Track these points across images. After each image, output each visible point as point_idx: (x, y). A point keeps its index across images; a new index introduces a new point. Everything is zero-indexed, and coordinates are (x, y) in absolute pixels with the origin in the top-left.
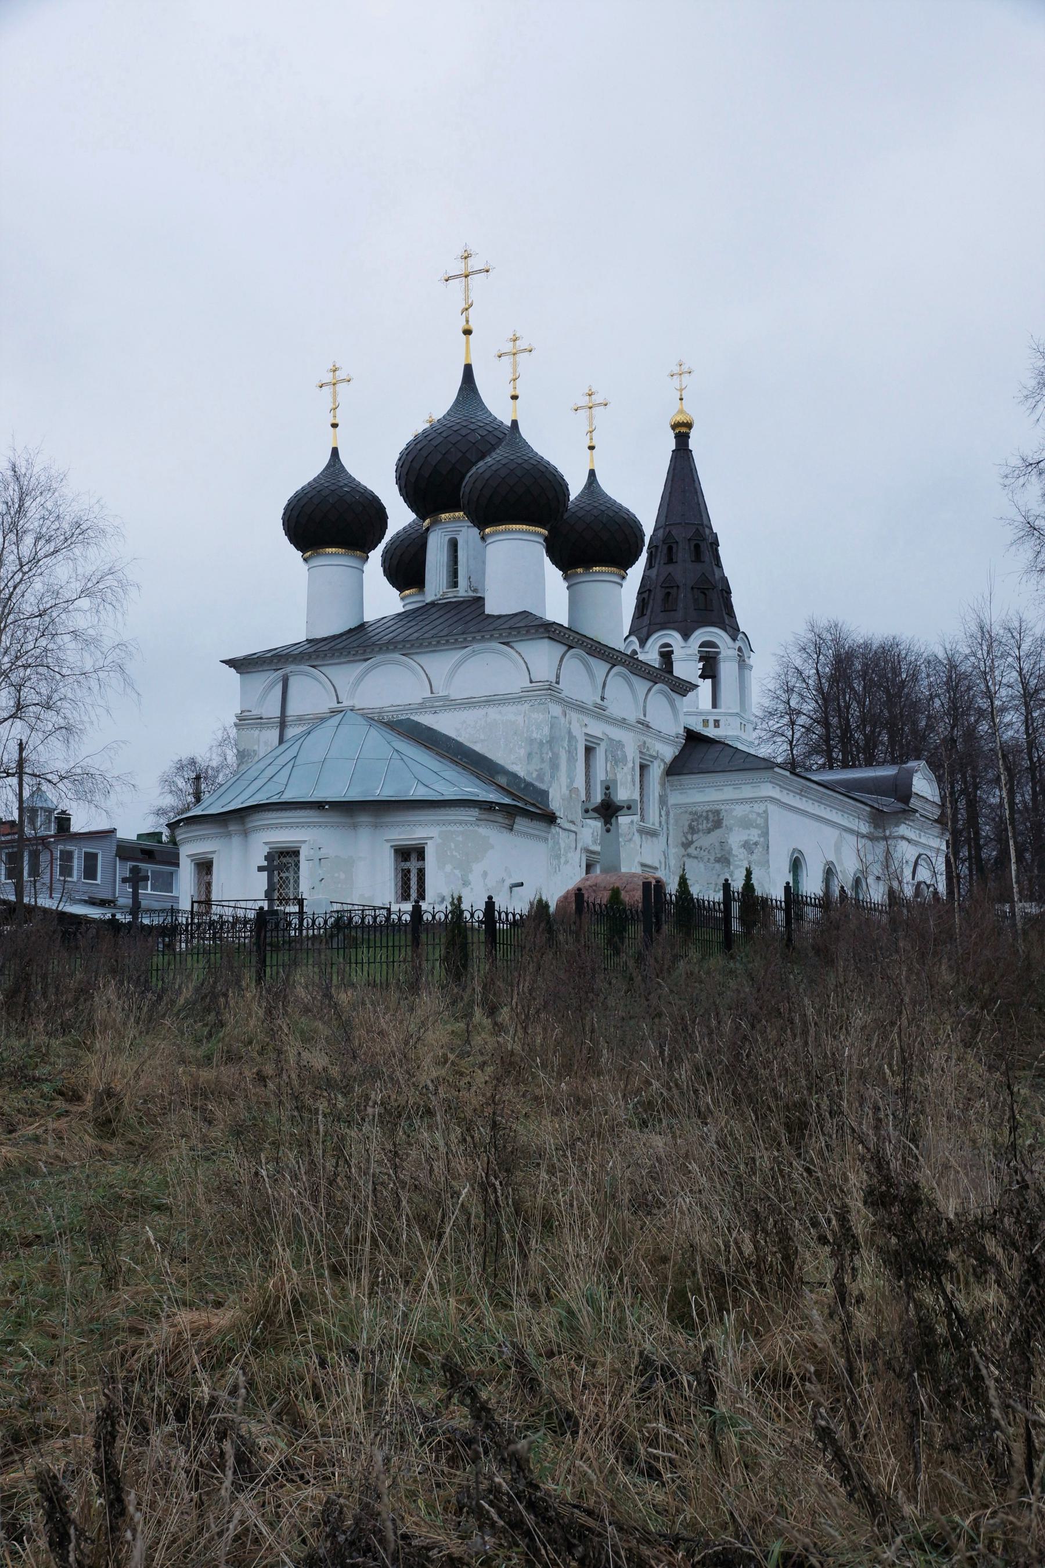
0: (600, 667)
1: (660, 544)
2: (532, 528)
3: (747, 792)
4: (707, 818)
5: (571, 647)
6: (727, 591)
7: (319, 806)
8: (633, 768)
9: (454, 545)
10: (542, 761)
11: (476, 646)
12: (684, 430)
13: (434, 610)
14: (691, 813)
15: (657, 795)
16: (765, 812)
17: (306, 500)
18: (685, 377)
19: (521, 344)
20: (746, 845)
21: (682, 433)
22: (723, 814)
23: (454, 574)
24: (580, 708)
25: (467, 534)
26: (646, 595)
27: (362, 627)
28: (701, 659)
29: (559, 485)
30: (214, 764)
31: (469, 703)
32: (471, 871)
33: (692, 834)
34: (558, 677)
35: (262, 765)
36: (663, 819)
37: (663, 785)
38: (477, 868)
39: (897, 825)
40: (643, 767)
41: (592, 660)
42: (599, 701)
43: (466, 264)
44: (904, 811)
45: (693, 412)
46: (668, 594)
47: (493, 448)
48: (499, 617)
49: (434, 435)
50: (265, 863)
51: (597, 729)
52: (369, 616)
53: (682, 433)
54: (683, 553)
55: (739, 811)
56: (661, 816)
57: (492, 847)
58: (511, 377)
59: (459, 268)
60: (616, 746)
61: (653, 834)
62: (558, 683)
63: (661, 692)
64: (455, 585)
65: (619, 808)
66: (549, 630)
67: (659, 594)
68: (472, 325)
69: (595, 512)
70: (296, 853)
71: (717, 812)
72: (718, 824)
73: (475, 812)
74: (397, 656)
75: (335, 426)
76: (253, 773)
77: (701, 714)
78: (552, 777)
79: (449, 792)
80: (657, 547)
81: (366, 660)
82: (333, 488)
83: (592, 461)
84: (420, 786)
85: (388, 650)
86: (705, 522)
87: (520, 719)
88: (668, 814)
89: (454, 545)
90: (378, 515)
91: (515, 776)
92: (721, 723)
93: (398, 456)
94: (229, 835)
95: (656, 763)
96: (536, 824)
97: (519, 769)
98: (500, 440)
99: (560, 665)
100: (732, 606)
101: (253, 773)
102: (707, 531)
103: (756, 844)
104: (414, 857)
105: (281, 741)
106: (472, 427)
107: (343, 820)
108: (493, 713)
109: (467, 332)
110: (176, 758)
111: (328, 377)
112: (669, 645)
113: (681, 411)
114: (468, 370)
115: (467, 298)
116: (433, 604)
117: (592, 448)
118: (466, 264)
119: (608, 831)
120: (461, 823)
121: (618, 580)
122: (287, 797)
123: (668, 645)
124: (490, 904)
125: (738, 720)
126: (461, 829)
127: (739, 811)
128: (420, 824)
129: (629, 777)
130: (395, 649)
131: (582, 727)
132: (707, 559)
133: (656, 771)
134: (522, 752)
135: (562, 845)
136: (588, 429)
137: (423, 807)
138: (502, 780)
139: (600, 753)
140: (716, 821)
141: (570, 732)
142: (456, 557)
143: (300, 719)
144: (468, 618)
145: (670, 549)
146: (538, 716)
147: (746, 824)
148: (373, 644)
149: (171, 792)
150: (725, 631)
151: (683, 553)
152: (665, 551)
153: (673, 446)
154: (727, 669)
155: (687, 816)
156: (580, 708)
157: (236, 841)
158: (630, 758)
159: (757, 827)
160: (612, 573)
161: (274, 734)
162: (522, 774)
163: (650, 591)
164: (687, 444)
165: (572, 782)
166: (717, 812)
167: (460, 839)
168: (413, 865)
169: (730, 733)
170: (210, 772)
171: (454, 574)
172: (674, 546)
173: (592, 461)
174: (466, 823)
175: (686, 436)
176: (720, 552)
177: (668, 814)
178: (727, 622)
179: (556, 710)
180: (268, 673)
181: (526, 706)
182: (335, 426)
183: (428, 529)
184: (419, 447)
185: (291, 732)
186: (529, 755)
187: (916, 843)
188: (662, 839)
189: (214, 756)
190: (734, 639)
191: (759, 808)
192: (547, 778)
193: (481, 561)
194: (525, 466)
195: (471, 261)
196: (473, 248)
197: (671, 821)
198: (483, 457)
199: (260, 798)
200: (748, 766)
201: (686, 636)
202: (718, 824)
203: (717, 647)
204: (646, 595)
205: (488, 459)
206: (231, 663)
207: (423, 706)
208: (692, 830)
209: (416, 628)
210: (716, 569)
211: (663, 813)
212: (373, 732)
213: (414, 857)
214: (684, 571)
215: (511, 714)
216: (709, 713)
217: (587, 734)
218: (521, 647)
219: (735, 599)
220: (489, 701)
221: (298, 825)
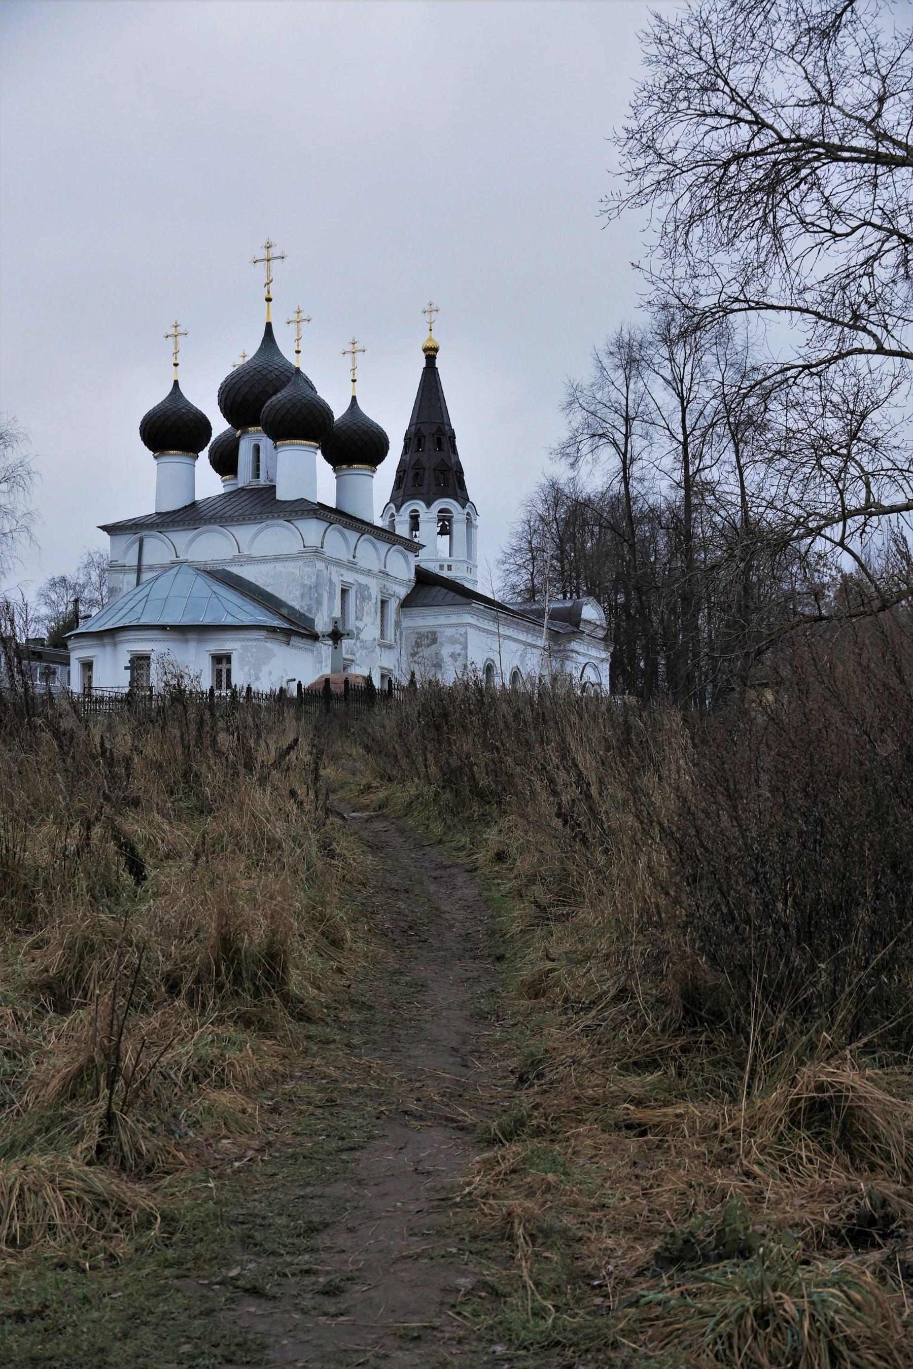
0: (353, 536)
1: (412, 437)
2: (308, 443)
3: (454, 619)
4: (427, 637)
5: (332, 524)
6: (461, 472)
7: (163, 628)
8: (376, 603)
9: (257, 449)
10: (311, 599)
11: (269, 522)
12: (432, 353)
13: (244, 493)
14: (417, 633)
15: (393, 621)
16: (466, 633)
17: (155, 418)
18: (434, 314)
19: (303, 316)
20: (453, 656)
21: (431, 354)
22: (438, 634)
23: (257, 468)
24: (338, 563)
25: (266, 443)
26: (401, 474)
27: (194, 504)
28: (440, 520)
29: (326, 412)
30: (81, 581)
31: (263, 560)
32: (261, 671)
33: (418, 647)
34: (322, 543)
35: (125, 600)
36: (398, 637)
37: (398, 615)
38: (265, 669)
39: (570, 642)
40: (383, 603)
41: (346, 531)
42: (351, 559)
43: (268, 252)
44: (574, 632)
45: (439, 340)
46: (417, 474)
47: (284, 385)
48: (285, 502)
49: (244, 373)
50: (129, 665)
51: (350, 577)
52: (199, 496)
53: (431, 354)
54: (429, 443)
55: (449, 632)
56: (396, 635)
57: (275, 656)
58: (296, 337)
59: (263, 254)
60: (363, 590)
61: (390, 647)
62: (322, 547)
63: (398, 551)
64: (258, 476)
65: (343, 635)
66: (319, 511)
67: (411, 473)
68: (272, 295)
69: (355, 427)
70: (148, 658)
71: (434, 633)
72: (434, 641)
73: (264, 633)
74: (216, 527)
75: (176, 365)
76: (120, 605)
77: (438, 560)
78: (317, 610)
79: (247, 620)
80: (410, 439)
81: (195, 529)
82: (175, 410)
83: (354, 390)
84: (229, 616)
85: (210, 523)
86: (446, 421)
87: (297, 571)
88: (401, 634)
89: (257, 449)
90: (204, 426)
91: (292, 608)
92: (453, 568)
93: (219, 386)
94: (104, 645)
95: (393, 599)
96: (305, 641)
97: (296, 605)
98: (289, 379)
99: (324, 536)
100: (464, 482)
101: (120, 605)
102: (447, 428)
103: (459, 655)
104: (224, 661)
105: (138, 584)
106: (270, 368)
107: (176, 637)
108: (279, 566)
109: (269, 300)
110: (50, 577)
111: (172, 331)
112: (417, 511)
113: (430, 339)
114: (269, 326)
115: (269, 276)
116: (242, 489)
117: (354, 381)
118: (268, 252)
119: (336, 648)
120: (255, 640)
121: (370, 473)
122: (143, 621)
123: (416, 511)
124: (249, 689)
125: (466, 566)
126: (254, 643)
127: (449, 632)
128: (228, 640)
129: (373, 609)
130: (215, 523)
131: (339, 576)
132: (446, 449)
133: (393, 605)
134: (298, 593)
135: (324, 654)
136: (352, 367)
137: (224, 630)
138: (285, 611)
139: (352, 594)
140: (433, 639)
141: (330, 580)
142: (258, 457)
143: (151, 568)
144: (266, 501)
145: (419, 441)
146: (308, 570)
147: (453, 641)
148: (201, 518)
149: (46, 603)
150: (458, 501)
151: (429, 443)
152: (416, 442)
153: (424, 364)
154: (459, 528)
155: (414, 635)
156: (338, 563)
157: (108, 649)
158: (374, 596)
159: (460, 643)
160: (366, 469)
161: (133, 577)
162: (297, 608)
163: (404, 471)
164: (434, 364)
165: (331, 613)
166: (434, 633)
167: (254, 650)
168: (224, 667)
169: (458, 575)
170: (77, 588)
171: (257, 468)
172: (423, 439)
173: (354, 390)
174: (258, 640)
175: (434, 357)
176: (457, 443)
177: (401, 634)
178: (459, 494)
179: (320, 565)
180: (127, 537)
181: (301, 563)
182: (176, 365)
183: (240, 437)
184: (234, 381)
185: (146, 576)
186: (303, 595)
187: (584, 655)
188: (397, 651)
189: (81, 576)
190: (463, 507)
191: (462, 630)
192: (314, 611)
193: (274, 460)
194: (304, 401)
195: (272, 250)
196: (273, 241)
197: (404, 639)
198: (277, 391)
199: (125, 622)
200: (455, 602)
201: (429, 504)
202: (434, 641)
203: (451, 512)
204: (401, 474)
205: (279, 395)
206: (104, 528)
207: (233, 561)
208: (418, 645)
209: (228, 503)
210: (452, 455)
211: (398, 633)
212: (199, 579)
213: (224, 661)
214: (430, 457)
215: (292, 568)
216: (445, 560)
217: (342, 581)
218: (297, 523)
219: (467, 478)
220: (277, 559)
221: (149, 640)
